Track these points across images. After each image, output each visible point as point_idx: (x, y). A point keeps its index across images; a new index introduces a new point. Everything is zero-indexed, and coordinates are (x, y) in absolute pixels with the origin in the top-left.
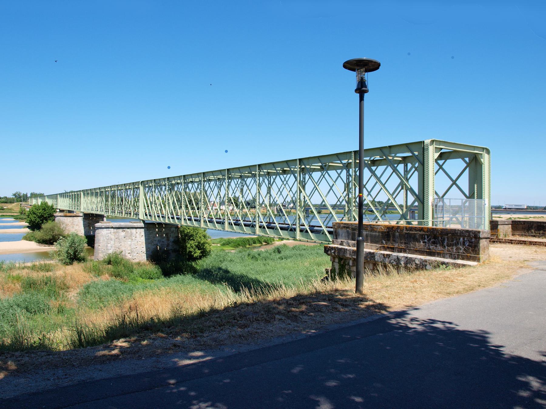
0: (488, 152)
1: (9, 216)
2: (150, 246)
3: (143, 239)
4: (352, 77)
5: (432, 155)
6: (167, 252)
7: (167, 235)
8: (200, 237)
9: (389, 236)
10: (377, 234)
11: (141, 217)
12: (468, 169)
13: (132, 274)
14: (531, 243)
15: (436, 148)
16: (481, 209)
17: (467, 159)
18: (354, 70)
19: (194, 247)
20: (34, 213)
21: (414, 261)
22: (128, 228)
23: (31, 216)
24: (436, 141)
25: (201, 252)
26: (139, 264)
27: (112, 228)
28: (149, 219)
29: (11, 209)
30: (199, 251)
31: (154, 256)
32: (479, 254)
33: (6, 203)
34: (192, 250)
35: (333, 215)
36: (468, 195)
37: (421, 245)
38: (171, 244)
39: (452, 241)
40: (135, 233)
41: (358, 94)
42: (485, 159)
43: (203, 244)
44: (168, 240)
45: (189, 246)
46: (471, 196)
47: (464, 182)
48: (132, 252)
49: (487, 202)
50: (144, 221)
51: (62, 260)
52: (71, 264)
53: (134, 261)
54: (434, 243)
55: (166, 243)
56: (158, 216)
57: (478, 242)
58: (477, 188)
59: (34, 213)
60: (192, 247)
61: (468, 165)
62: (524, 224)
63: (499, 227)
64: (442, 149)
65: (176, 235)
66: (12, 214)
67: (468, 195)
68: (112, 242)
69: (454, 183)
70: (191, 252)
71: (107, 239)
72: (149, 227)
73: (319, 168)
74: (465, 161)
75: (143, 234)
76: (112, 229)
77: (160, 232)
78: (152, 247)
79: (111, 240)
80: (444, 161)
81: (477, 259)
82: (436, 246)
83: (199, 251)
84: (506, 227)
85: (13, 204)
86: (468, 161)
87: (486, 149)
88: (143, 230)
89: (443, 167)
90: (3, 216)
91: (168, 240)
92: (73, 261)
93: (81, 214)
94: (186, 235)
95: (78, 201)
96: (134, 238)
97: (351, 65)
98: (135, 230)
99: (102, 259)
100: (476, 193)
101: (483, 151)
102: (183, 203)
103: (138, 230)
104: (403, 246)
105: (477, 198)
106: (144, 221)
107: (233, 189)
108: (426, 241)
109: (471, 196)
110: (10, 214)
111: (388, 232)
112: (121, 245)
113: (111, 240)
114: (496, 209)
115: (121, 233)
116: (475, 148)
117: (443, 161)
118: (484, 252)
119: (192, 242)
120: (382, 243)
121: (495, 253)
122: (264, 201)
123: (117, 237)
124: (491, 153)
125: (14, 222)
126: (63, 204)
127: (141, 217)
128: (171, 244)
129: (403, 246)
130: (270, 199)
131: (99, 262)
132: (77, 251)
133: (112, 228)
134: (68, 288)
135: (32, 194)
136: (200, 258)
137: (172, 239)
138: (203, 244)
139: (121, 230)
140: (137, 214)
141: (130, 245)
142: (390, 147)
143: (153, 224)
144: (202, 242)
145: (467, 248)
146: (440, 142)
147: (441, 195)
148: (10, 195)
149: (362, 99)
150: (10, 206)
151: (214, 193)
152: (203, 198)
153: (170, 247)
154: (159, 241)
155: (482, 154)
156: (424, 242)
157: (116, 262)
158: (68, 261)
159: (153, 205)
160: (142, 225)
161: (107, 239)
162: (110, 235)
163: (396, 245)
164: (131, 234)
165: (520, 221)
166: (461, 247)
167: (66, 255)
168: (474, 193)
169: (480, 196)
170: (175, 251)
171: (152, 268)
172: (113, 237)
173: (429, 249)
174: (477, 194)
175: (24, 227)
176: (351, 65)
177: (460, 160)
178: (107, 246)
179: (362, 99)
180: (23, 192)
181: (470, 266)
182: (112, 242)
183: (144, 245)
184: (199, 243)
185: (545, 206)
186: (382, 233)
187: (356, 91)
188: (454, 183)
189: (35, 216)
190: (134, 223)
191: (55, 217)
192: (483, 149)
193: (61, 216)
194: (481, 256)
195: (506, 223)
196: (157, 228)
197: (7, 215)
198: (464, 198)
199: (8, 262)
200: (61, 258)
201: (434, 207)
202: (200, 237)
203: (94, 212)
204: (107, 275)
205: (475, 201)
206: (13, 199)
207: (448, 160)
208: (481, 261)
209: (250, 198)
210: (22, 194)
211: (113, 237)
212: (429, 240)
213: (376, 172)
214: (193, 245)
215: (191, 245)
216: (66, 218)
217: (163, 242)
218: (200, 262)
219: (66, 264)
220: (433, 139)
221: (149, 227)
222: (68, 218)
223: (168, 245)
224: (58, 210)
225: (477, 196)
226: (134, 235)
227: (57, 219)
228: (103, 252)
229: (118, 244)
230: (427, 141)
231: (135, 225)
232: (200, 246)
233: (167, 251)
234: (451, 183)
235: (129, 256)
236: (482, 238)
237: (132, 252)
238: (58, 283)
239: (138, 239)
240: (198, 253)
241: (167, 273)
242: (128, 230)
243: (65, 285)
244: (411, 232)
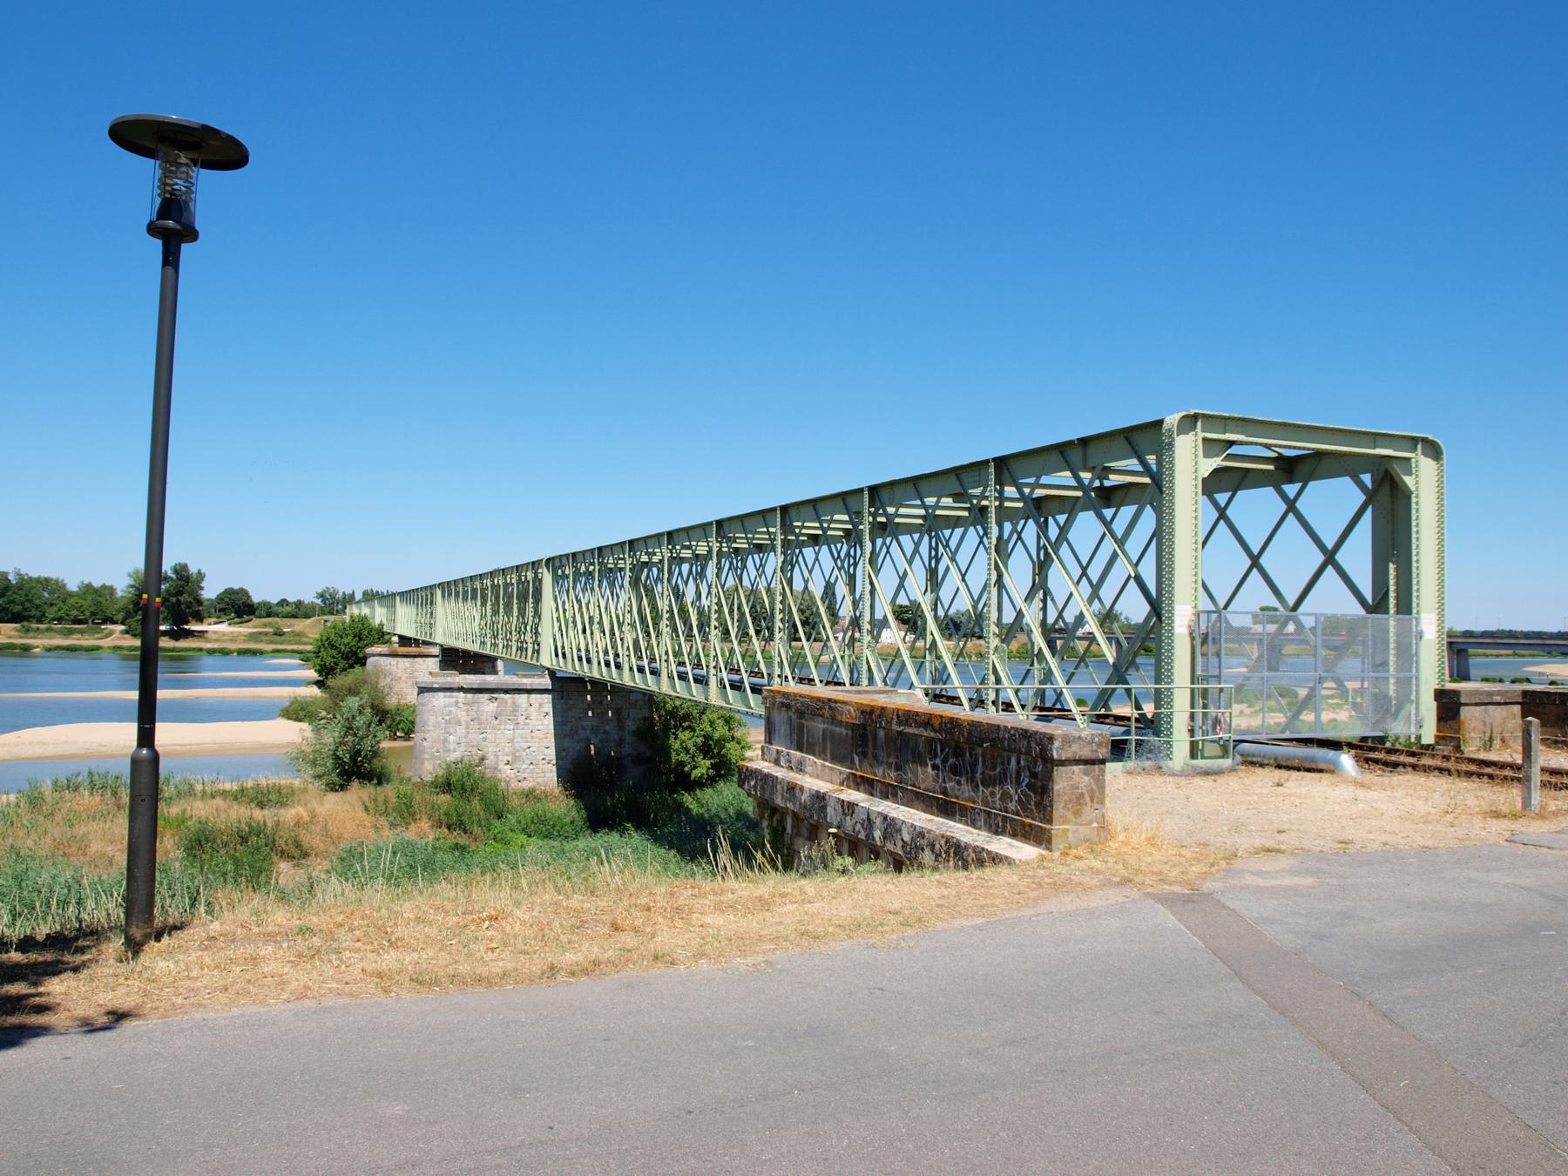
0: (1433, 450)
1: (293, 651)
2: (567, 743)
3: (549, 723)
4: (140, 177)
5: (1190, 462)
6: (616, 765)
8: (712, 723)
9: (872, 742)
10: (844, 731)
11: (547, 659)
12: (1369, 513)
13: (496, 823)
15: (1205, 440)
16: (1407, 655)
17: (1367, 478)
18: (149, 153)
19: (693, 749)
20: (332, 646)
21: (899, 831)
22: (507, 691)
23: (324, 653)
24: (1205, 416)
25: (713, 766)
26: (530, 795)
27: (461, 689)
28: (570, 668)
29: (299, 634)
30: (708, 763)
31: (580, 774)
32: (1050, 821)
33: (295, 616)
34: (684, 757)
36: (1369, 598)
37: (925, 776)
38: (629, 739)
39: (993, 769)
40: (525, 705)
41: (159, 242)
42: (1423, 479)
43: (721, 743)
44: (621, 727)
45: (676, 745)
46: (1377, 606)
47: (1358, 556)
48: (516, 759)
49: (1429, 627)
50: (552, 673)
51: (319, 777)
52: (343, 787)
53: (514, 785)
54: (955, 771)
55: (614, 735)
56: (607, 664)
57: (1049, 777)
58: (1397, 577)
59: (332, 646)
60: (687, 751)
61: (1371, 497)
62: (1563, 702)
63: (1466, 713)
64: (1232, 443)
65: (646, 713)
66: (301, 647)
67: (1369, 598)
68: (461, 731)
69: (1330, 558)
70: (682, 764)
72: (566, 688)
73: (966, 514)
75: (549, 708)
77: (598, 703)
78: (574, 747)
80: (1299, 485)
81: (1039, 837)
82: (959, 783)
83: (708, 763)
84: (1497, 713)
85: (308, 621)
86: (1369, 485)
87: (1424, 440)
88: (548, 698)
89: (1298, 505)
90: (278, 651)
91: (621, 727)
92: (349, 780)
93: (436, 650)
94: (673, 713)
95: (522, 613)
96: (521, 719)
97: (134, 135)
98: (524, 696)
99: (429, 778)
100: (1392, 595)
101: (1414, 450)
102: (778, 624)
103: (533, 696)
104: (891, 777)
105: (1398, 612)
106: (552, 673)
108: (938, 761)
109: (1377, 606)
110: (295, 647)
111: (863, 726)
112: (485, 739)
114: (1460, 649)
115: (487, 705)
116: (1376, 438)
117: (1298, 486)
118: (1077, 813)
119: (684, 735)
120: (852, 765)
121: (1145, 813)
122: (1020, 614)
124: (1445, 456)
125: (300, 667)
126: (405, 621)
129: (891, 777)
130: (1044, 609)
131: (422, 785)
132: (359, 752)
133: (461, 689)
134: (305, 855)
135: (365, 594)
136: (712, 781)
137: (631, 725)
138: (721, 743)
139: (487, 696)
141: (512, 740)
142: (1084, 442)
143: (579, 681)
144: (716, 735)
145: (1026, 795)
146: (1226, 422)
147: (1291, 603)
148: (309, 597)
149: (171, 259)
150: (300, 625)
152: (779, 606)
153: (626, 749)
154: (594, 730)
155: (1409, 459)
156: (935, 767)
157: (463, 787)
158: (337, 780)
159: (596, 627)
160: (546, 682)
163: (879, 773)
164: (516, 708)
165: (1548, 694)
166: (1012, 791)
167: (330, 763)
168: (1387, 592)
169: (1405, 607)
170: (639, 759)
171: (564, 807)
172: (462, 715)
173: (944, 792)
174: (1397, 597)
175: (308, 683)
176: (134, 135)
177: (1346, 481)
178: (446, 740)
179: (171, 259)
180: (343, 588)
181: (996, 859)
182: (461, 731)
184: (707, 737)
186: (853, 727)
187: (152, 229)
188: (1330, 558)
189: (335, 653)
190: (525, 676)
191: (365, 658)
192: (1415, 440)
193: (380, 655)
194: (1057, 828)
195: (1498, 699)
196: (589, 692)
197: (285, 651)
198: (1361, 611)
200: (320, 770)
201: (1198, 642)
202: (712, 723)
204: (425, 825)
205: (1392, 621)
206: (313, 606)
207: (1312, 484)
208: (1057, 843)
209: (964, 604)
210: (340, 595)
211: (462, 715)
212: (944, 761)
214: (690, 744)
215: (682, 742)
216: (393, 661)
217: (606, 732)
218: (707, 795)
219: (333, 788)
220: (1192, 412)
221: (566, 688)
222: (401, 660)
224: (396, 639)
225: (1397, 605)
227: (370, 661)
228: (433, 758)
229: (476, 737)
230: (1172, 420)
231: (527, 682)
232: (708, 748)
233: (619, 759)
234: (1321, 558)
235: (507, 772)
236: (1062, 763)
237: (516, 759)
238: (282, 842)
239: (533, 722)
240: (703, 767)
241: (599, 820)
242: (507, 696)
243: (298, 845)
244: (908, 730)
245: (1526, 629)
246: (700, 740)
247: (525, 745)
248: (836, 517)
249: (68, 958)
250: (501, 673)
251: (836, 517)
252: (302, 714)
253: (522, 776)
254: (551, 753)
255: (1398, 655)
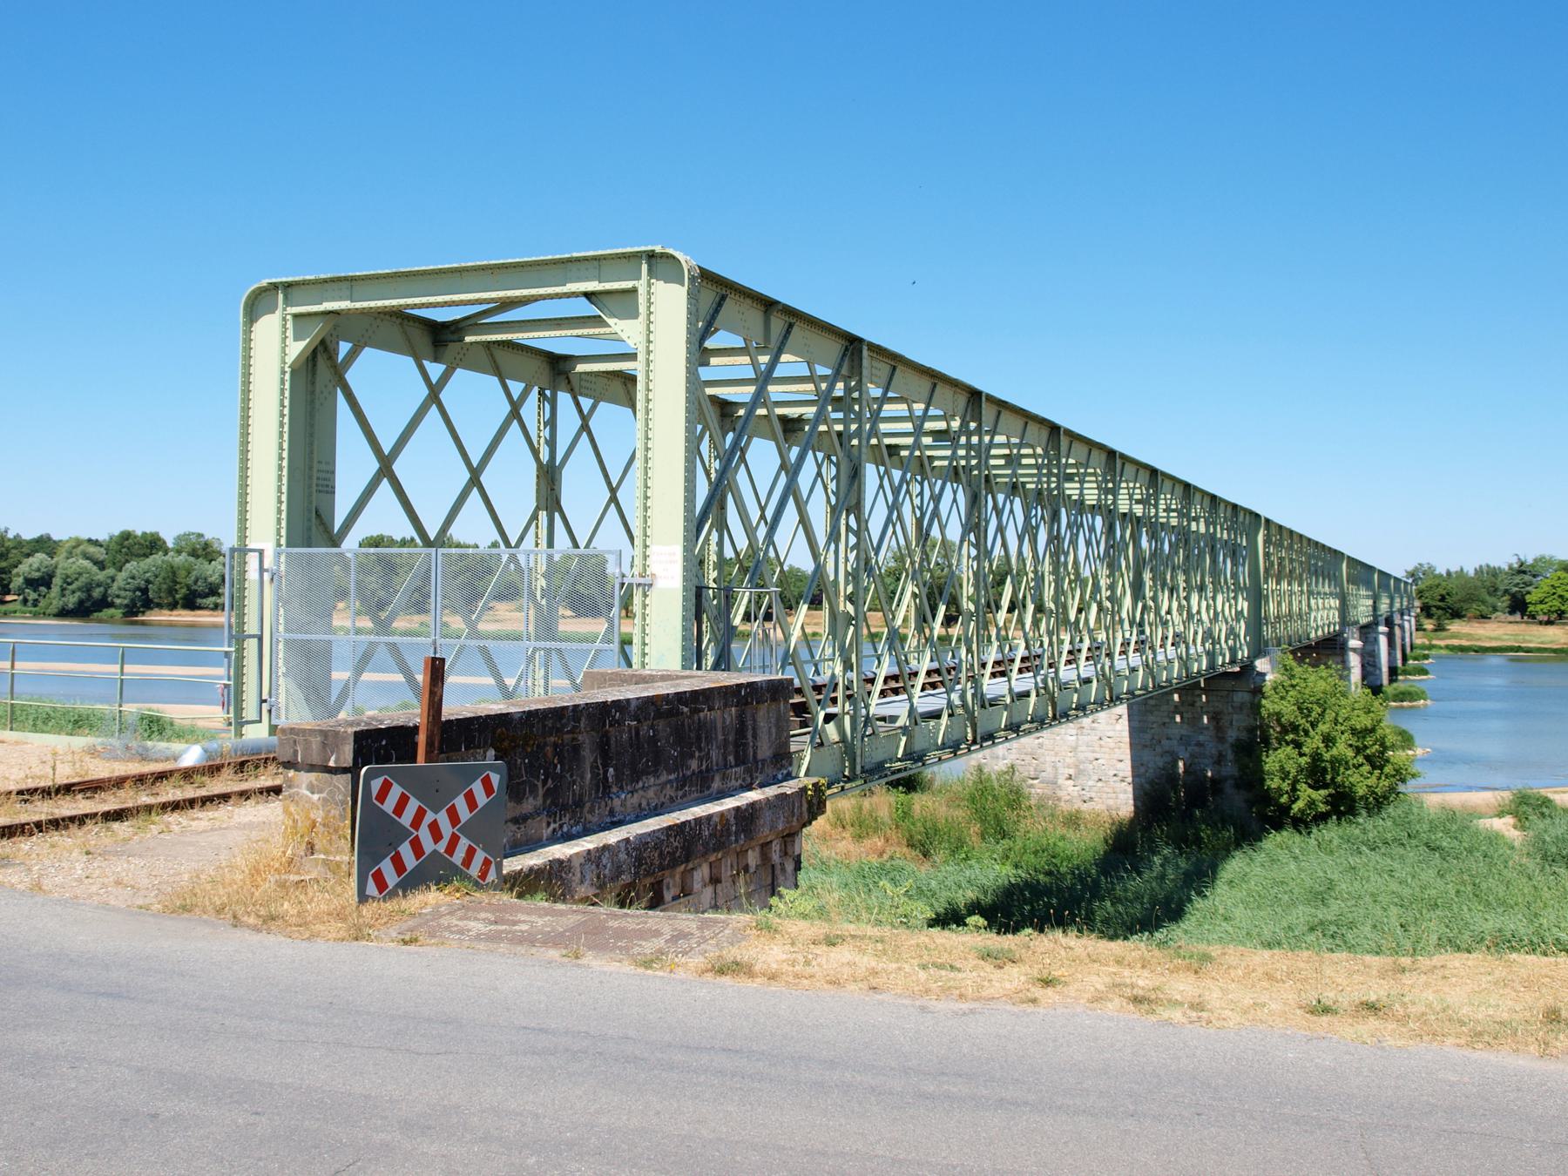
2: (1147, 756)
7: (1215, 718)
14: (56, 824)
15: (295, 316)
35: (559, 651)
38: (1230, 756)
44: (1221, 739)
48: (1080, 772)
55: (1212, 749)
74: (352, 355)
78: (1156, 761)
91: (1221, 739)
112: (1041, 746)
141: (1074, 749)
183: (1125, 753)
184: (1316, 757)
185: (1563, 558)
188: (386, 469)
197: (580, 641)
217: (1199, 744)
223: (1219, 760)
237: (1080, 772)
245: (1328, 544)
246: (1303, 761)
247: (1092, 756)
248: (946, 463)
249: (507, 916)
250: (421, 761)
251: (946, 463)
252: (1370, 669)
253: (1087, 795)
254: (1126, 768)
255: (637, 848)
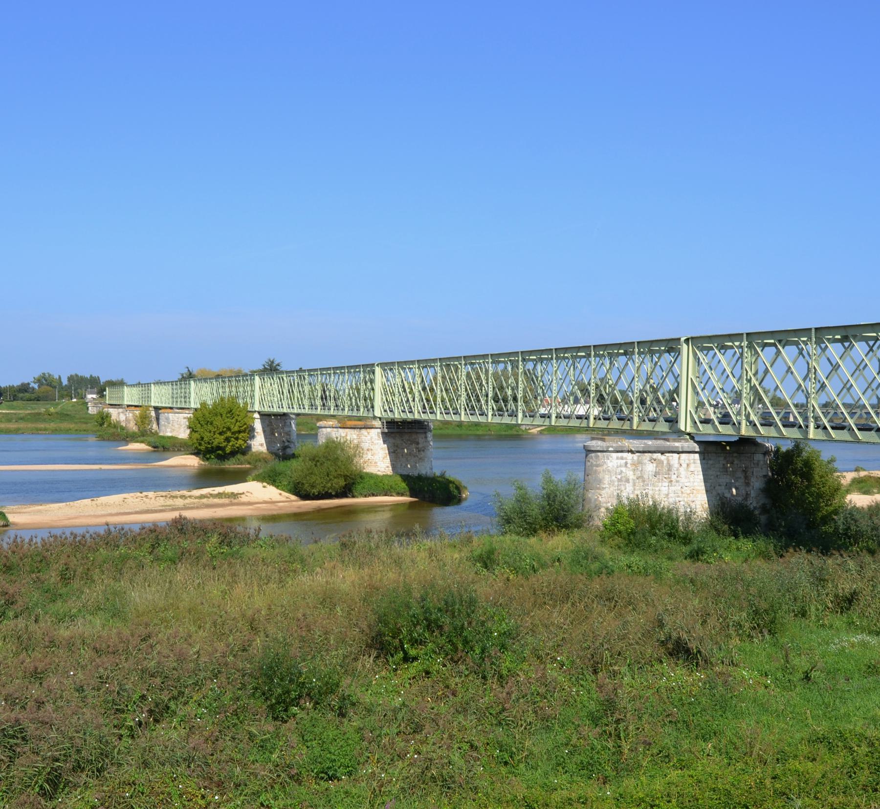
71: (620, 480)
72: (710, 450)
76: (629, 456)
79: (628, 481)
96: (674, 477)
103: (683, 456)
107: (592, 371)
113: (628, 481)
123: (638, 473)
127: (684, 424)
128: (753, 494)
140: (672, 421)
151: (557, 377)
161: (620, 480)
162: (624, 469)
172: (631, 475)
190: (675, 440)
199: (670, 575)
203: (276, 410)
211: (631, 475)
213: (840, 344)
226: (674, 469)
